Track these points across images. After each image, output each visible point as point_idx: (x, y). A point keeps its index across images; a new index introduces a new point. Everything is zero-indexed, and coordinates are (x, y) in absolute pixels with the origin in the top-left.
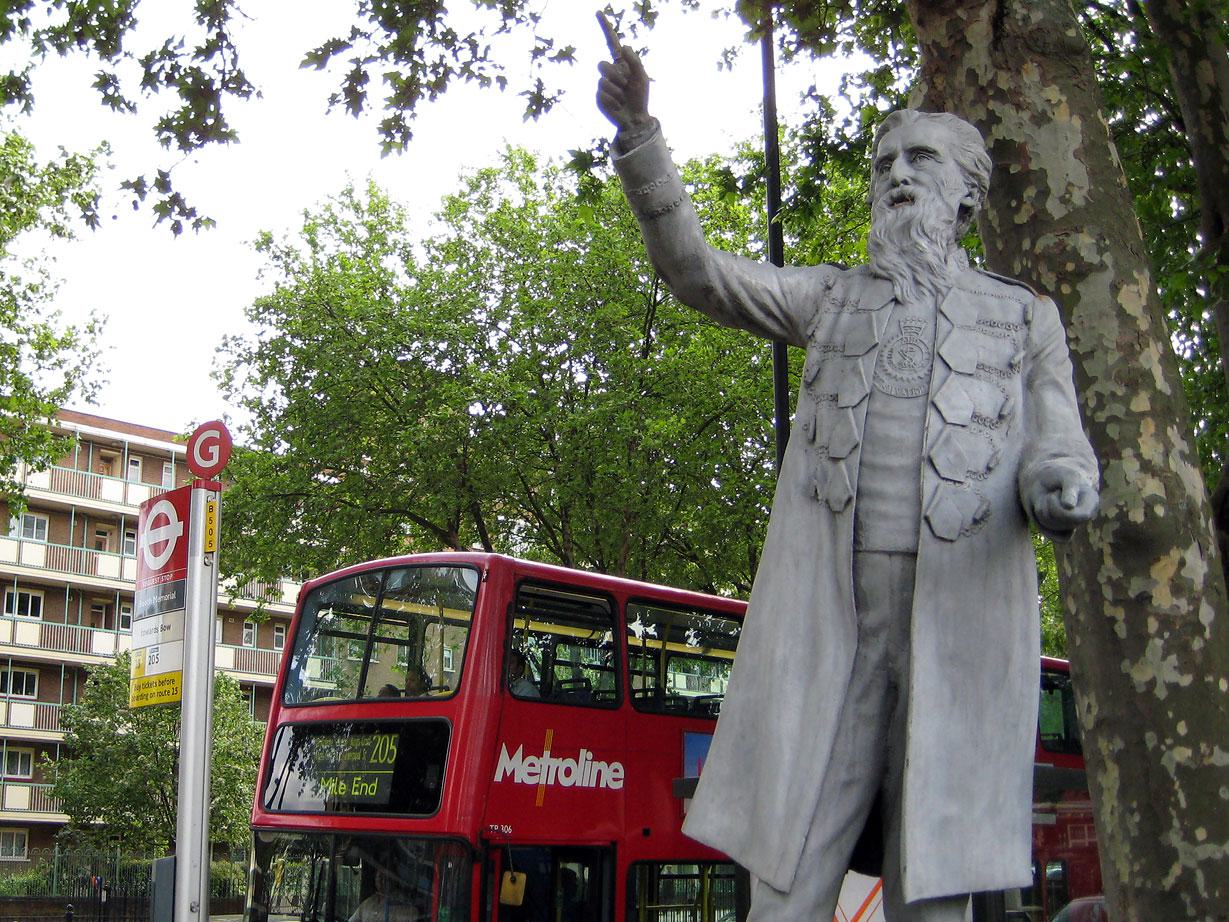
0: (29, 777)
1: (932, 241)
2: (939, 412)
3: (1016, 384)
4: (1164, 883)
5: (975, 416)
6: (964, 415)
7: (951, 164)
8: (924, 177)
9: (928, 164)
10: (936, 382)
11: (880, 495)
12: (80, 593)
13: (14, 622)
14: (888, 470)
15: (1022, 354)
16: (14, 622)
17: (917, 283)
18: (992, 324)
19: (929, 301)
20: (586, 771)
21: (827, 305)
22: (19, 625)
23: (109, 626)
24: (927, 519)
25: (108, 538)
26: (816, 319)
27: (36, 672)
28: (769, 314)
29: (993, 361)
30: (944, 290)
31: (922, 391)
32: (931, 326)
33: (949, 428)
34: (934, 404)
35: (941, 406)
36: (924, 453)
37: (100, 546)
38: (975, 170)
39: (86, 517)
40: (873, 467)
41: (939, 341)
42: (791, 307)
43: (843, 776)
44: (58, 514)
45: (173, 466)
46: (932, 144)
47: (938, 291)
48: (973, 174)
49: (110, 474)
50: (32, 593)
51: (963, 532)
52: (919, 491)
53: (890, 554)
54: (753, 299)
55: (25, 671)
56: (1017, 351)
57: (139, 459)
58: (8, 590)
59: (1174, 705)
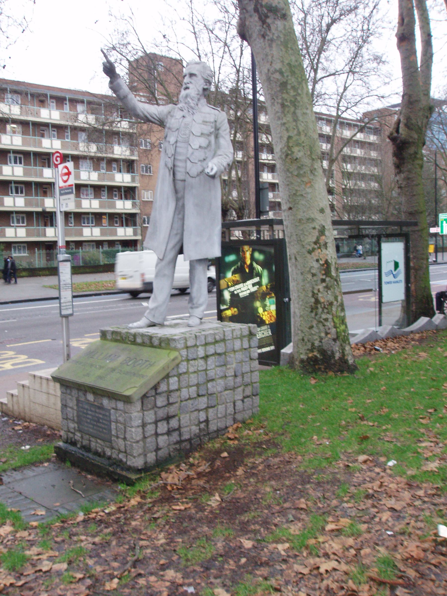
0: (25, 225)
3: (212, 138)
5: (200, 147)
6: (197, 147)
8: (192, 81)
9: (194, 78)
11: (179, 167)
12: (36, 154)
13: (13, 167)
14: (180, 160)
16: (13, 167)
18: (207, 122)
22: (15, 168)
23: (49, 166)
25: (45, 132)
27: (23, 186)
29: (205, 132)
37: (43, 136)
39: (36, 125)
40: (178, 160)
42: (161, 117)
43: (175, 232)
44: (24, 124)
45: (67, 102)
49: (44, 107)
50: (18, 156)
51: (198, 175)
55: (19, 185)
57: (54, 101)
58: (9, 155)
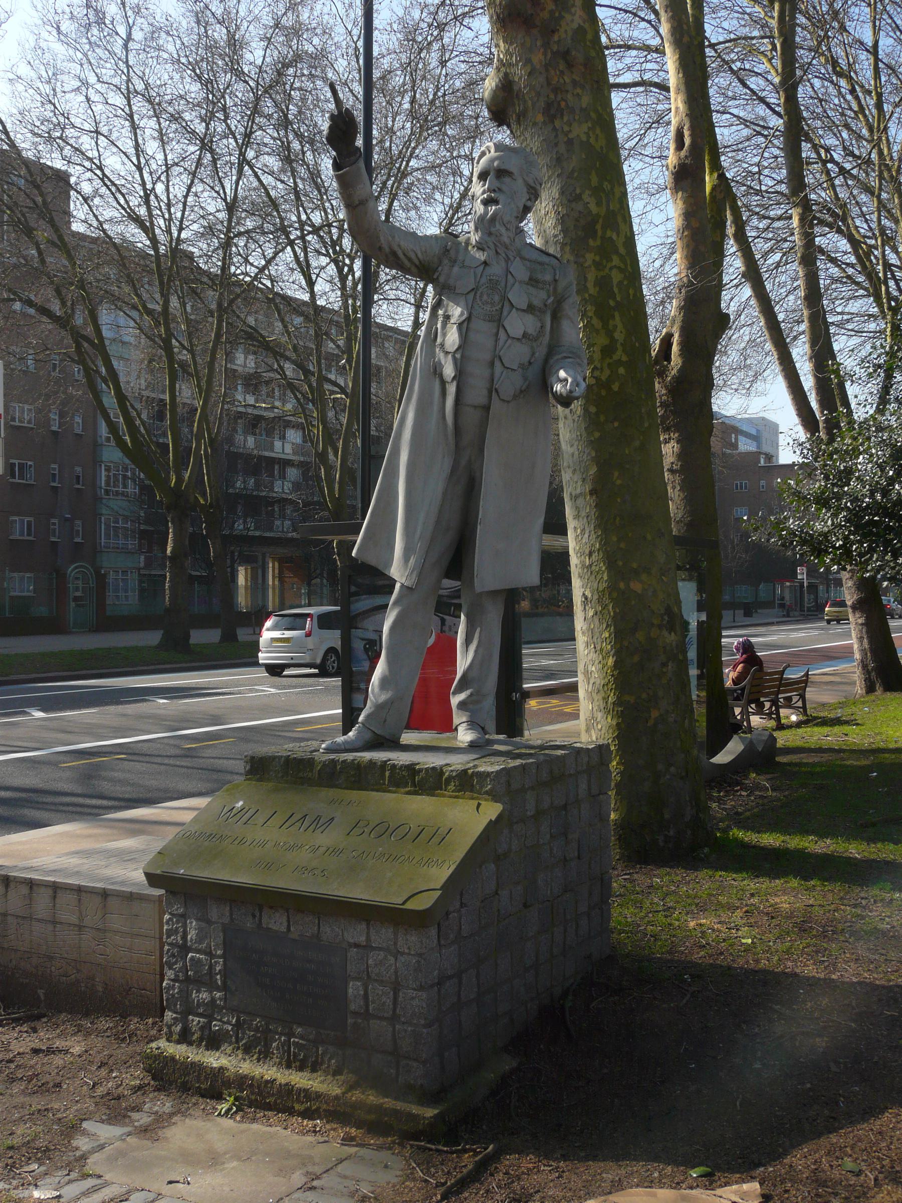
1: (507, 229)
2: (506, 330)
4: (403, 736)
7: (520, 181)
8: (504, 188)
9: (507, 180)
10: (505, 313)
15: (552, 299)
17: (497, 252)
19: (503, 264)
20: (675, 506)
21: (446, 261)
24: (496, 390)
26: (440, 269)
28: (410, 259)
30: (512, 258)
31: (497, 317)
32: (504, 280)
33: (510, 341)
34: (503, 326)
35: (508, 328)
36: (497, 352)
38: (533, 185)
41: (508, 289)
46: (511, 170)
47: (509, 259)
48: (532, 187)
52: (492, 375)
53: (475, 407)
54: (404, 254)
56: (549, 297)
59: (231, 491)
